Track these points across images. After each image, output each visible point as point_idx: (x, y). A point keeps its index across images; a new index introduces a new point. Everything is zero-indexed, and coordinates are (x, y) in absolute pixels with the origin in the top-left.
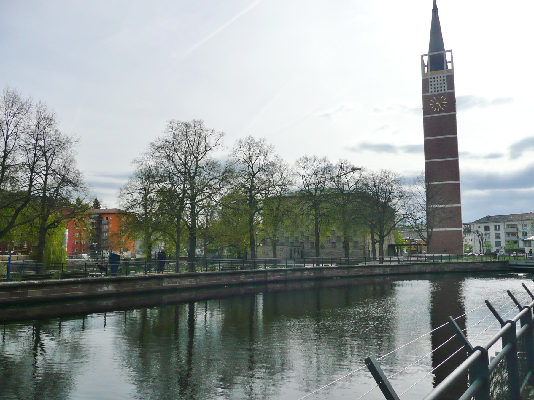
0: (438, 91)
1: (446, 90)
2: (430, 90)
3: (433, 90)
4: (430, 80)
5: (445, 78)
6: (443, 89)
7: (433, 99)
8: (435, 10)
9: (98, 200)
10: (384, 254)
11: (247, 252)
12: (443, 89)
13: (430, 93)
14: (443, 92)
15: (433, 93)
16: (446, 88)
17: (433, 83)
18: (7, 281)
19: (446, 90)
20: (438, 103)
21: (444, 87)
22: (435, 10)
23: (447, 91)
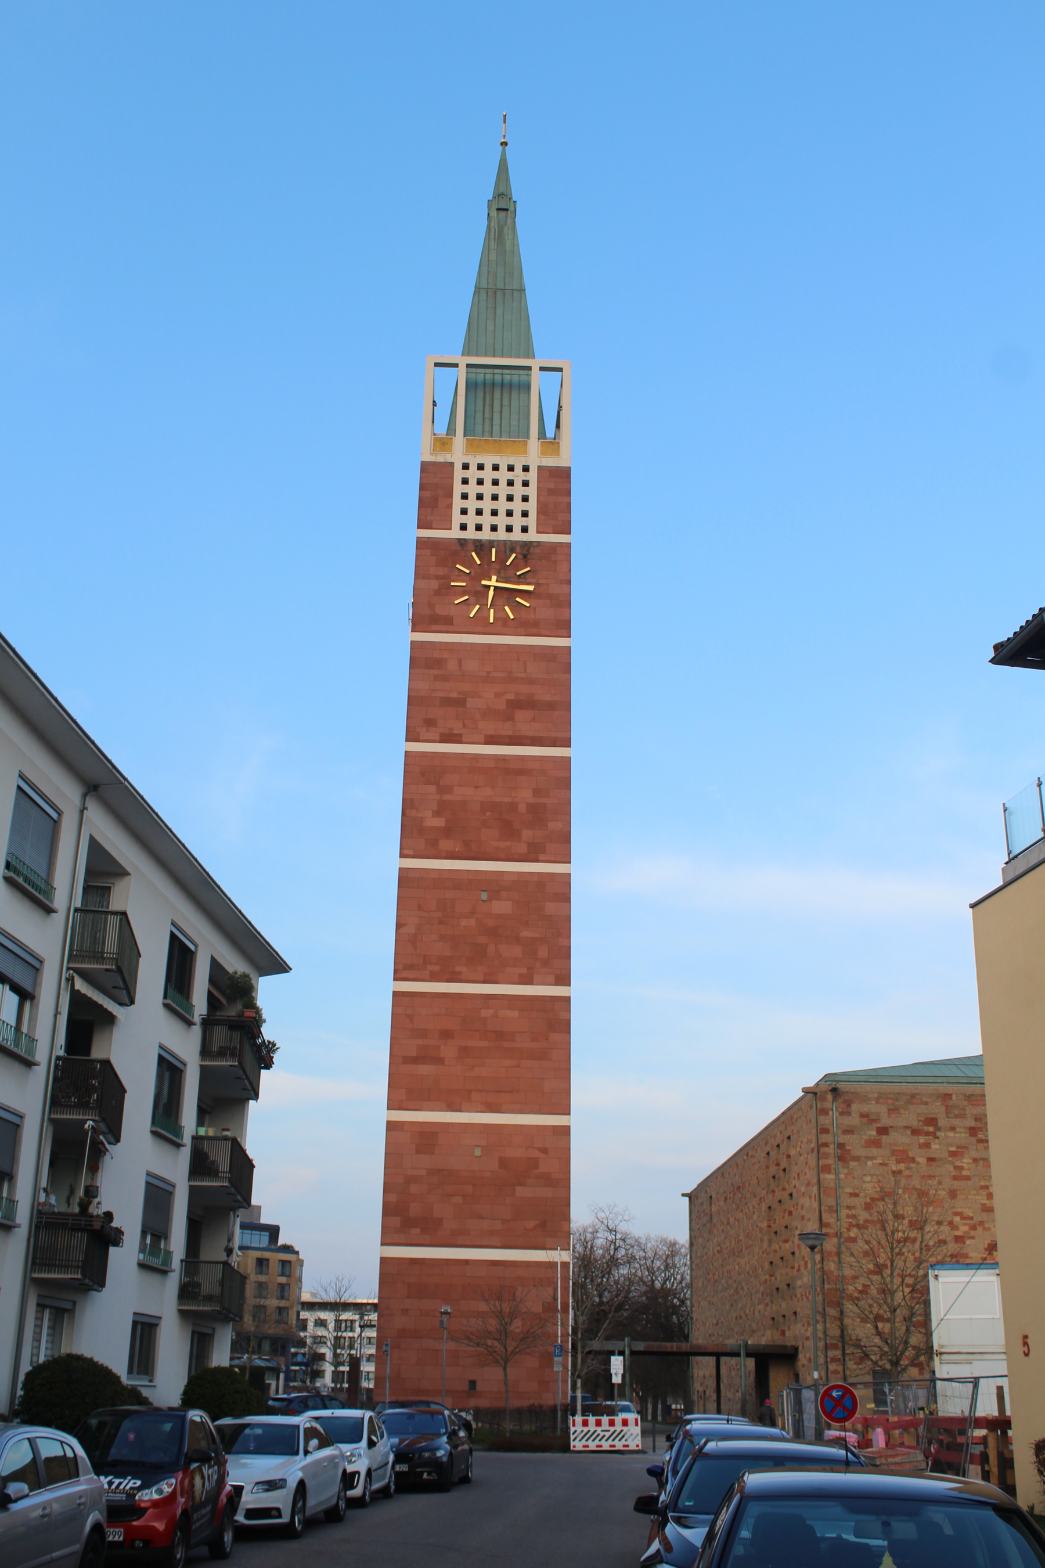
0: (494, 528)
1: (533, 528)
2: (457, 519)
3: (471, 519)
4: (459, 474)
5: (532, 476)
6: (517, 521)
7: (470, 563)
8: (502, 206)
9: (53, 914)
10: (663, 1344)
11: (254, 1316)
12: (517, 521)
13: (455, 533)
14: (517, 536)
15: (471, 534)
16: (532, 521)
17: (518, 491)
18: (846, 1465)
19: (533, 528)
20: (493, 582)
21: (525, 514)
22: (502, 206)
23: (532, 536)
